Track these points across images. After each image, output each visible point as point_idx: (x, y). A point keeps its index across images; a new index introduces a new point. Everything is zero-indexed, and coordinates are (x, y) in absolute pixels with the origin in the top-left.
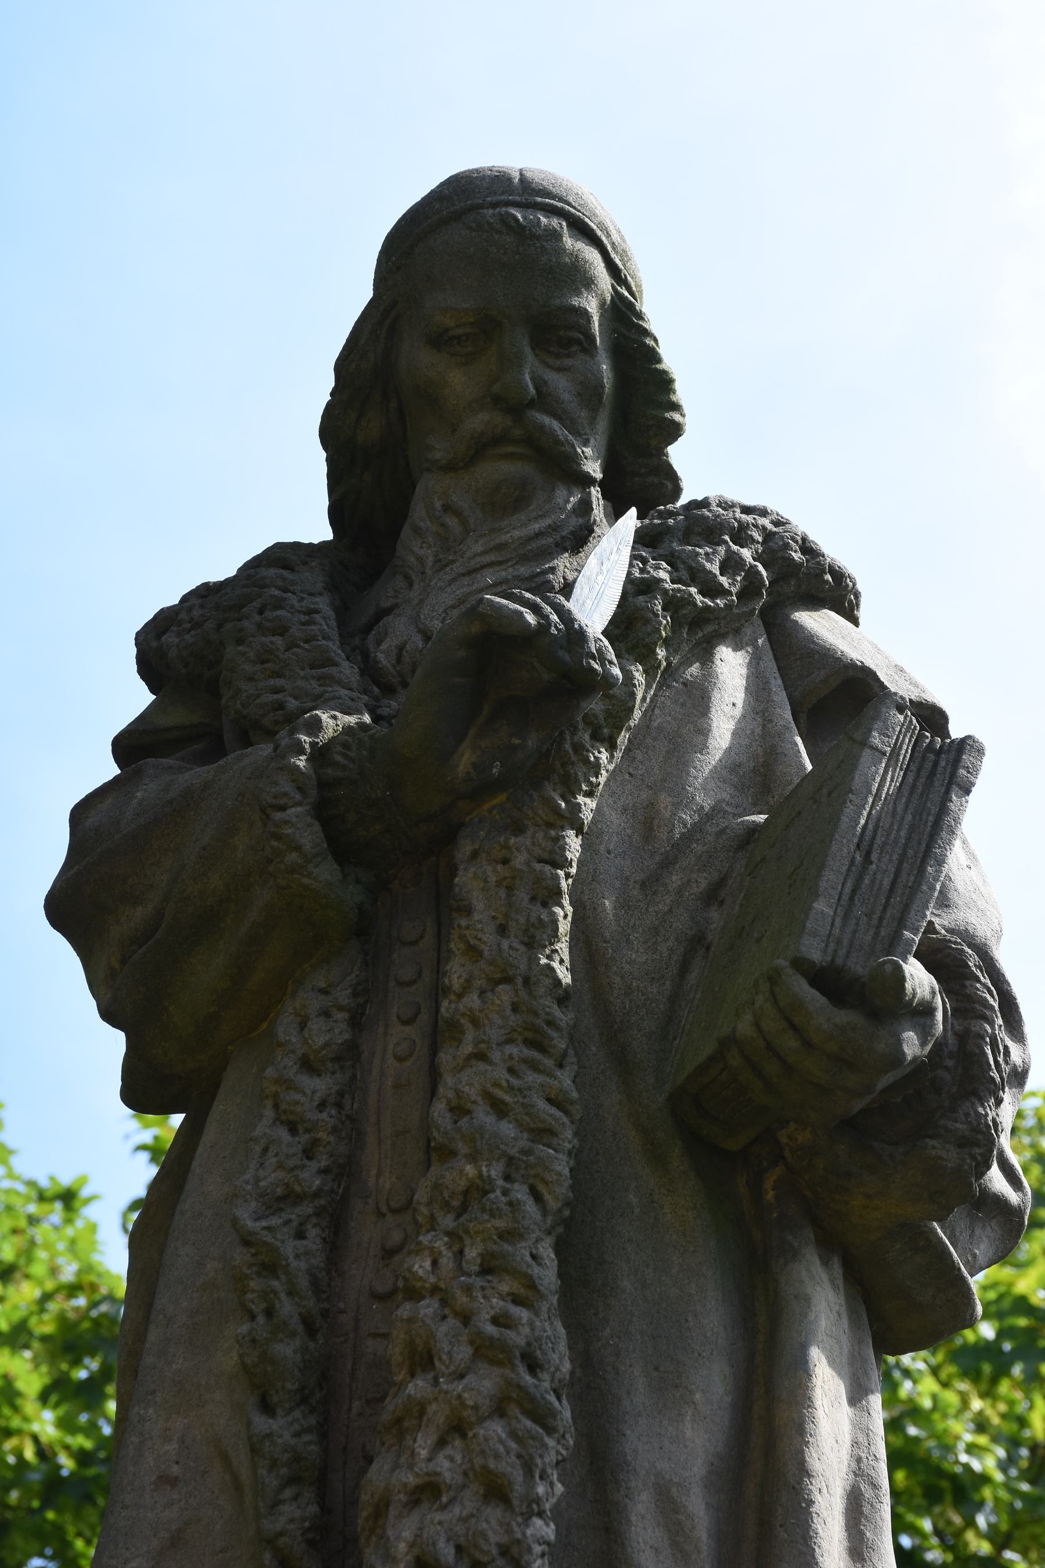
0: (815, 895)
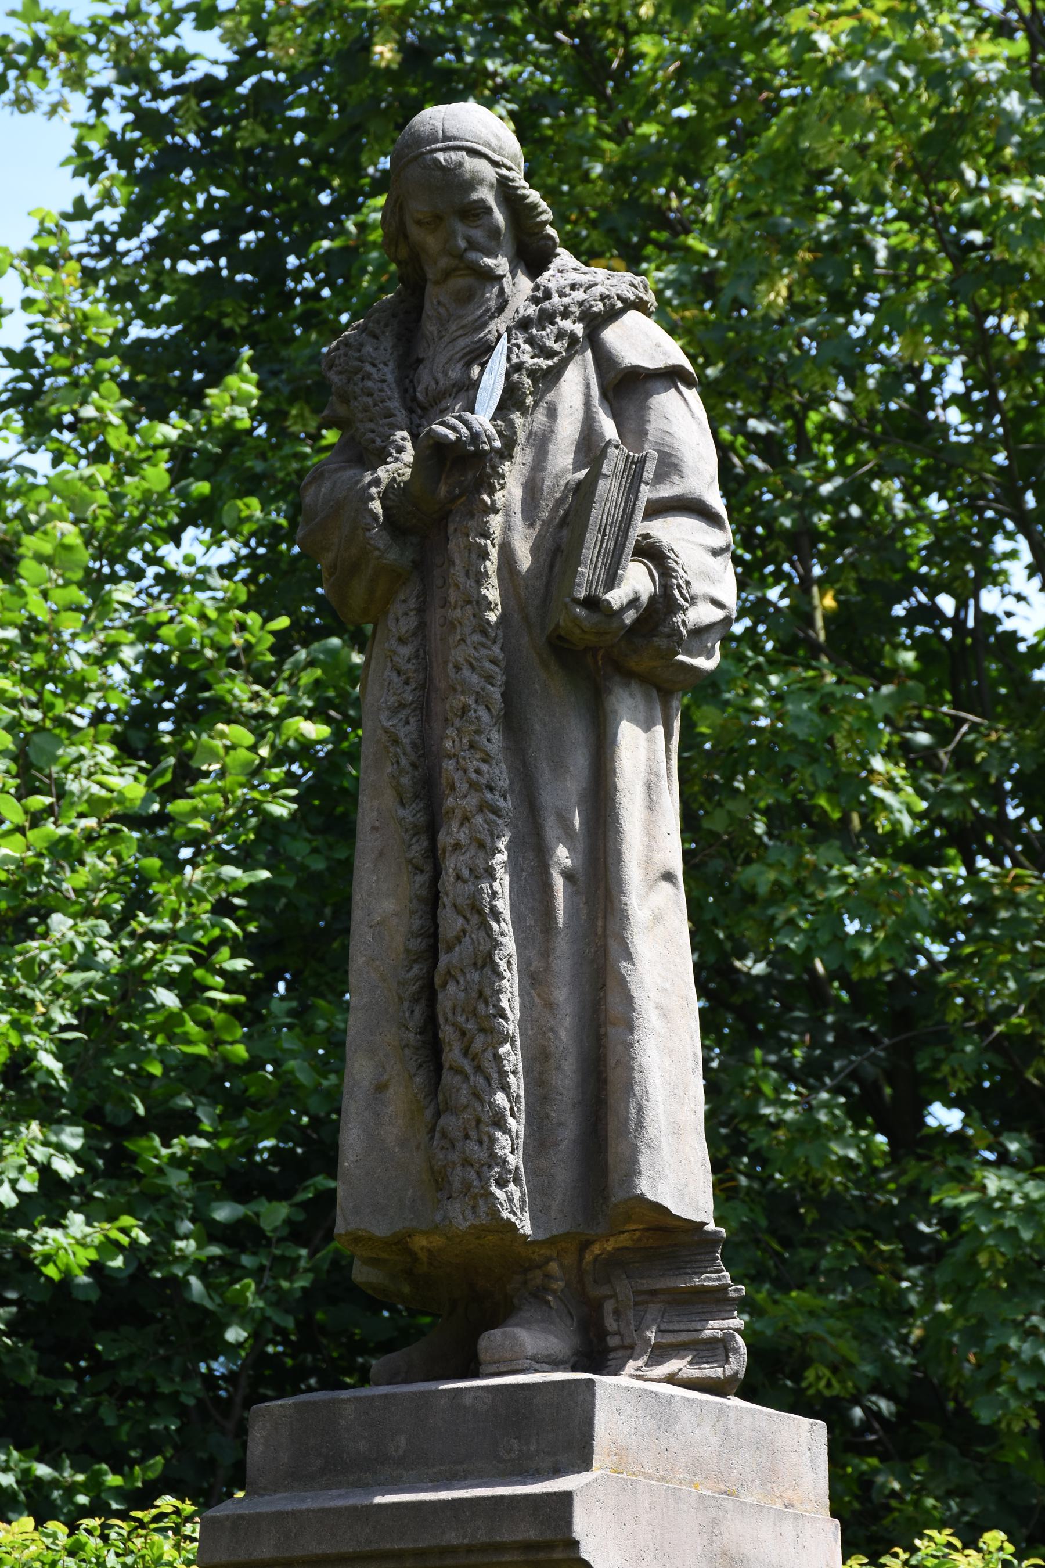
0: (579, 564)
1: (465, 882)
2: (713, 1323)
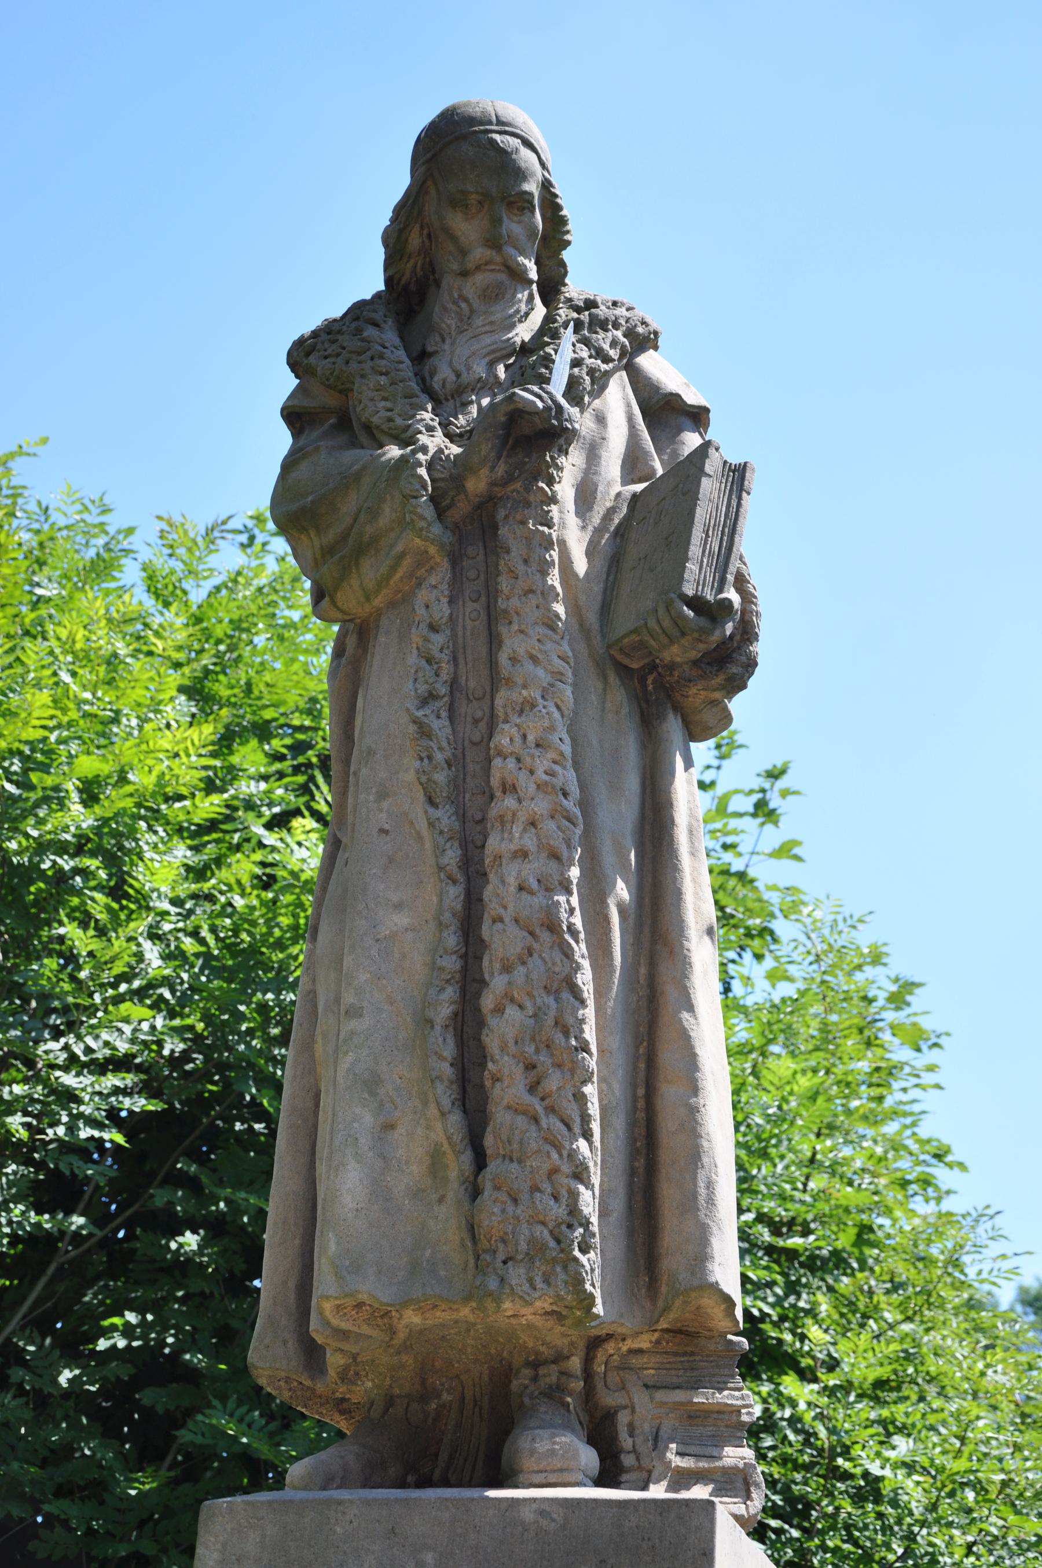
1: (532, 893)
2: (729, 1450)
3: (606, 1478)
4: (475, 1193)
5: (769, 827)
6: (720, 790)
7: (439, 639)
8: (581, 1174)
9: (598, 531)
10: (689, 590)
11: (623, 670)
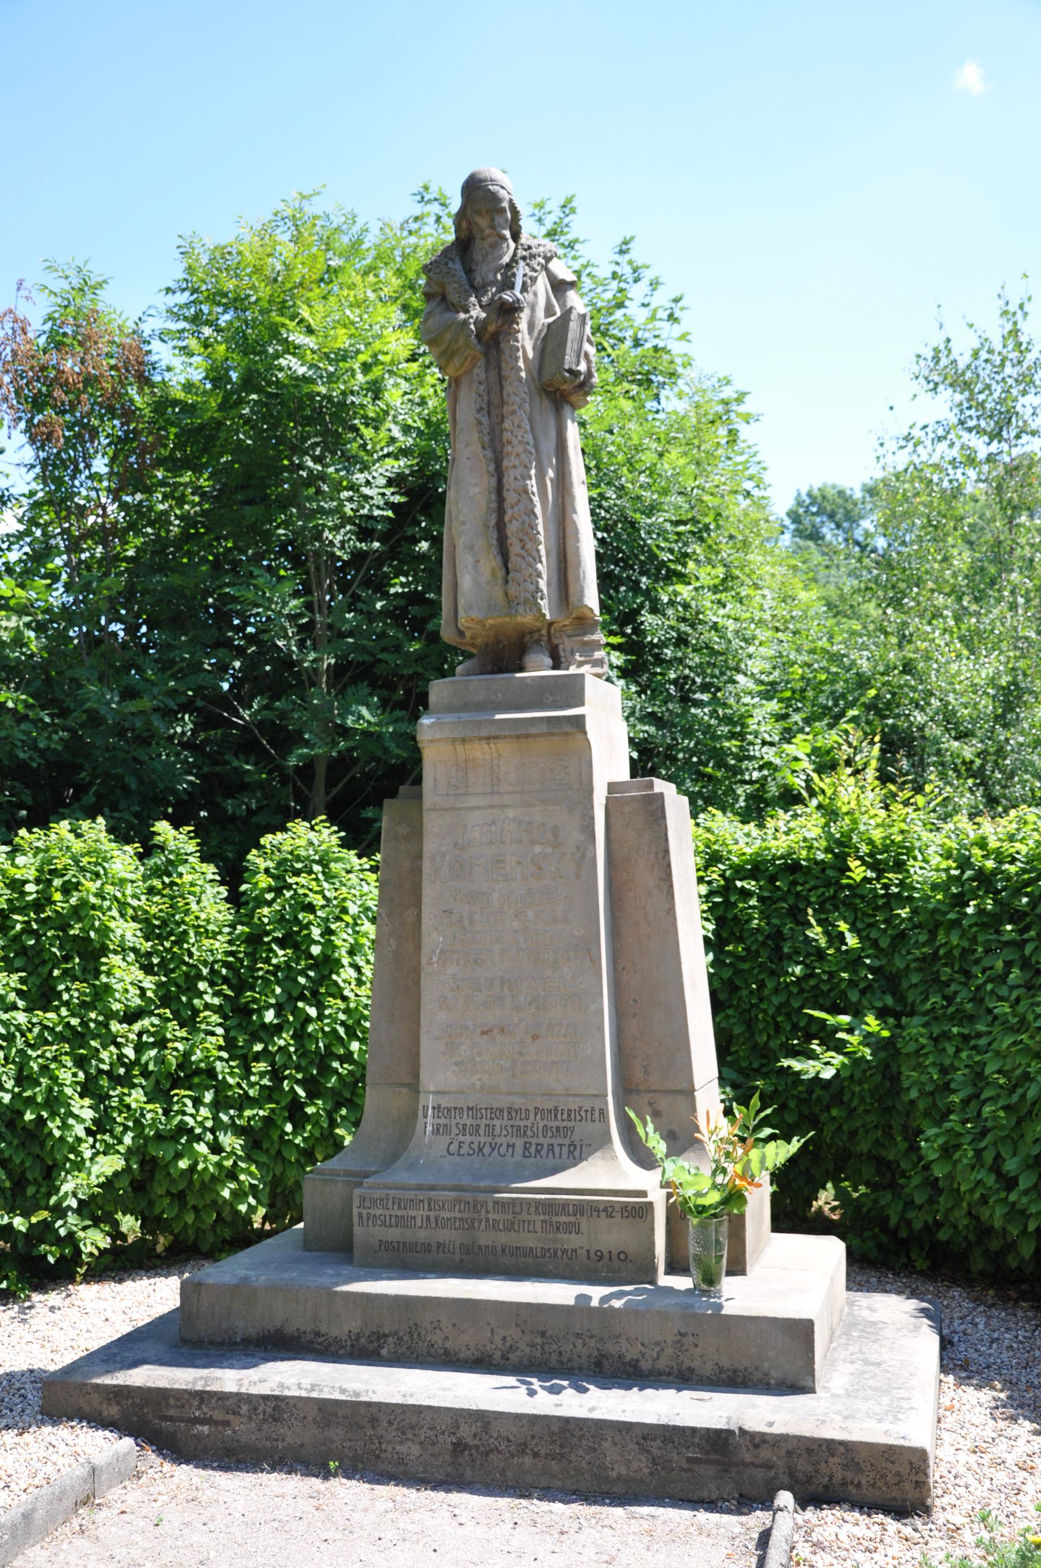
3: (556, 666)
4: (507, 582)
5: (676, 325)
6: (652, 306)
7: (482, 387)
8: (539, 575)
9: (537, 339)
10: (567, 367)
11: (546, 392)
